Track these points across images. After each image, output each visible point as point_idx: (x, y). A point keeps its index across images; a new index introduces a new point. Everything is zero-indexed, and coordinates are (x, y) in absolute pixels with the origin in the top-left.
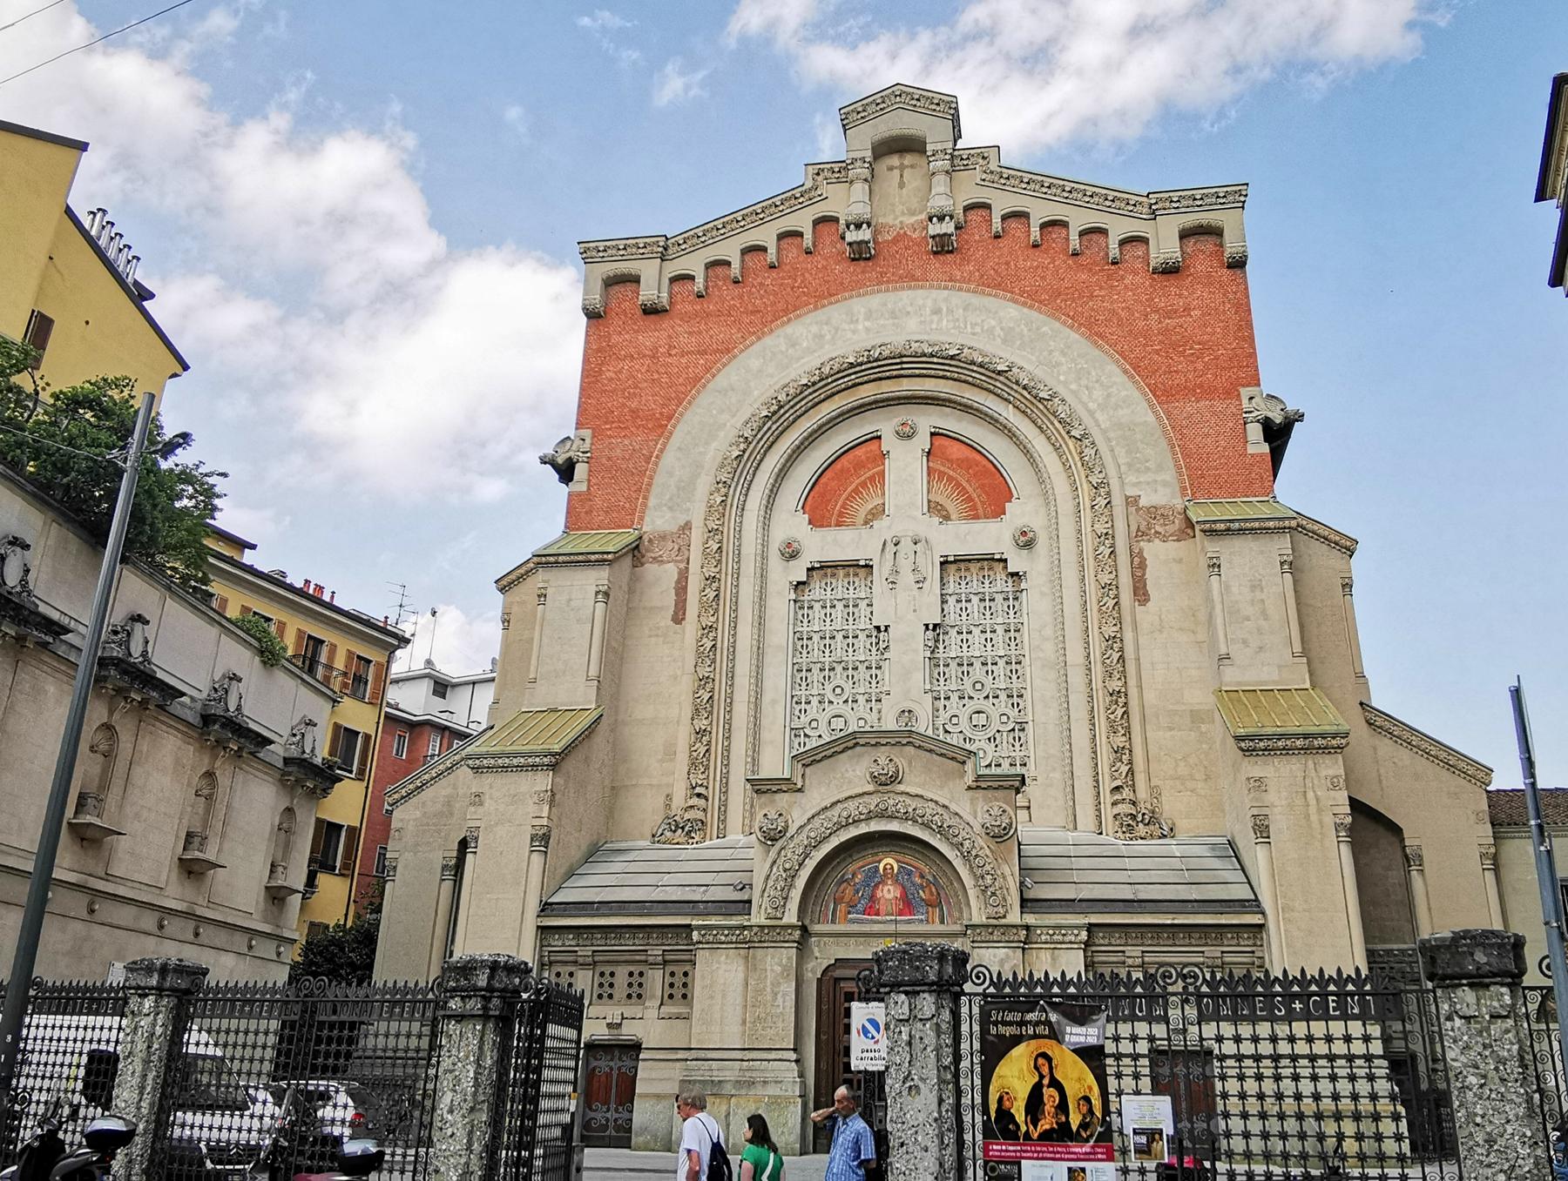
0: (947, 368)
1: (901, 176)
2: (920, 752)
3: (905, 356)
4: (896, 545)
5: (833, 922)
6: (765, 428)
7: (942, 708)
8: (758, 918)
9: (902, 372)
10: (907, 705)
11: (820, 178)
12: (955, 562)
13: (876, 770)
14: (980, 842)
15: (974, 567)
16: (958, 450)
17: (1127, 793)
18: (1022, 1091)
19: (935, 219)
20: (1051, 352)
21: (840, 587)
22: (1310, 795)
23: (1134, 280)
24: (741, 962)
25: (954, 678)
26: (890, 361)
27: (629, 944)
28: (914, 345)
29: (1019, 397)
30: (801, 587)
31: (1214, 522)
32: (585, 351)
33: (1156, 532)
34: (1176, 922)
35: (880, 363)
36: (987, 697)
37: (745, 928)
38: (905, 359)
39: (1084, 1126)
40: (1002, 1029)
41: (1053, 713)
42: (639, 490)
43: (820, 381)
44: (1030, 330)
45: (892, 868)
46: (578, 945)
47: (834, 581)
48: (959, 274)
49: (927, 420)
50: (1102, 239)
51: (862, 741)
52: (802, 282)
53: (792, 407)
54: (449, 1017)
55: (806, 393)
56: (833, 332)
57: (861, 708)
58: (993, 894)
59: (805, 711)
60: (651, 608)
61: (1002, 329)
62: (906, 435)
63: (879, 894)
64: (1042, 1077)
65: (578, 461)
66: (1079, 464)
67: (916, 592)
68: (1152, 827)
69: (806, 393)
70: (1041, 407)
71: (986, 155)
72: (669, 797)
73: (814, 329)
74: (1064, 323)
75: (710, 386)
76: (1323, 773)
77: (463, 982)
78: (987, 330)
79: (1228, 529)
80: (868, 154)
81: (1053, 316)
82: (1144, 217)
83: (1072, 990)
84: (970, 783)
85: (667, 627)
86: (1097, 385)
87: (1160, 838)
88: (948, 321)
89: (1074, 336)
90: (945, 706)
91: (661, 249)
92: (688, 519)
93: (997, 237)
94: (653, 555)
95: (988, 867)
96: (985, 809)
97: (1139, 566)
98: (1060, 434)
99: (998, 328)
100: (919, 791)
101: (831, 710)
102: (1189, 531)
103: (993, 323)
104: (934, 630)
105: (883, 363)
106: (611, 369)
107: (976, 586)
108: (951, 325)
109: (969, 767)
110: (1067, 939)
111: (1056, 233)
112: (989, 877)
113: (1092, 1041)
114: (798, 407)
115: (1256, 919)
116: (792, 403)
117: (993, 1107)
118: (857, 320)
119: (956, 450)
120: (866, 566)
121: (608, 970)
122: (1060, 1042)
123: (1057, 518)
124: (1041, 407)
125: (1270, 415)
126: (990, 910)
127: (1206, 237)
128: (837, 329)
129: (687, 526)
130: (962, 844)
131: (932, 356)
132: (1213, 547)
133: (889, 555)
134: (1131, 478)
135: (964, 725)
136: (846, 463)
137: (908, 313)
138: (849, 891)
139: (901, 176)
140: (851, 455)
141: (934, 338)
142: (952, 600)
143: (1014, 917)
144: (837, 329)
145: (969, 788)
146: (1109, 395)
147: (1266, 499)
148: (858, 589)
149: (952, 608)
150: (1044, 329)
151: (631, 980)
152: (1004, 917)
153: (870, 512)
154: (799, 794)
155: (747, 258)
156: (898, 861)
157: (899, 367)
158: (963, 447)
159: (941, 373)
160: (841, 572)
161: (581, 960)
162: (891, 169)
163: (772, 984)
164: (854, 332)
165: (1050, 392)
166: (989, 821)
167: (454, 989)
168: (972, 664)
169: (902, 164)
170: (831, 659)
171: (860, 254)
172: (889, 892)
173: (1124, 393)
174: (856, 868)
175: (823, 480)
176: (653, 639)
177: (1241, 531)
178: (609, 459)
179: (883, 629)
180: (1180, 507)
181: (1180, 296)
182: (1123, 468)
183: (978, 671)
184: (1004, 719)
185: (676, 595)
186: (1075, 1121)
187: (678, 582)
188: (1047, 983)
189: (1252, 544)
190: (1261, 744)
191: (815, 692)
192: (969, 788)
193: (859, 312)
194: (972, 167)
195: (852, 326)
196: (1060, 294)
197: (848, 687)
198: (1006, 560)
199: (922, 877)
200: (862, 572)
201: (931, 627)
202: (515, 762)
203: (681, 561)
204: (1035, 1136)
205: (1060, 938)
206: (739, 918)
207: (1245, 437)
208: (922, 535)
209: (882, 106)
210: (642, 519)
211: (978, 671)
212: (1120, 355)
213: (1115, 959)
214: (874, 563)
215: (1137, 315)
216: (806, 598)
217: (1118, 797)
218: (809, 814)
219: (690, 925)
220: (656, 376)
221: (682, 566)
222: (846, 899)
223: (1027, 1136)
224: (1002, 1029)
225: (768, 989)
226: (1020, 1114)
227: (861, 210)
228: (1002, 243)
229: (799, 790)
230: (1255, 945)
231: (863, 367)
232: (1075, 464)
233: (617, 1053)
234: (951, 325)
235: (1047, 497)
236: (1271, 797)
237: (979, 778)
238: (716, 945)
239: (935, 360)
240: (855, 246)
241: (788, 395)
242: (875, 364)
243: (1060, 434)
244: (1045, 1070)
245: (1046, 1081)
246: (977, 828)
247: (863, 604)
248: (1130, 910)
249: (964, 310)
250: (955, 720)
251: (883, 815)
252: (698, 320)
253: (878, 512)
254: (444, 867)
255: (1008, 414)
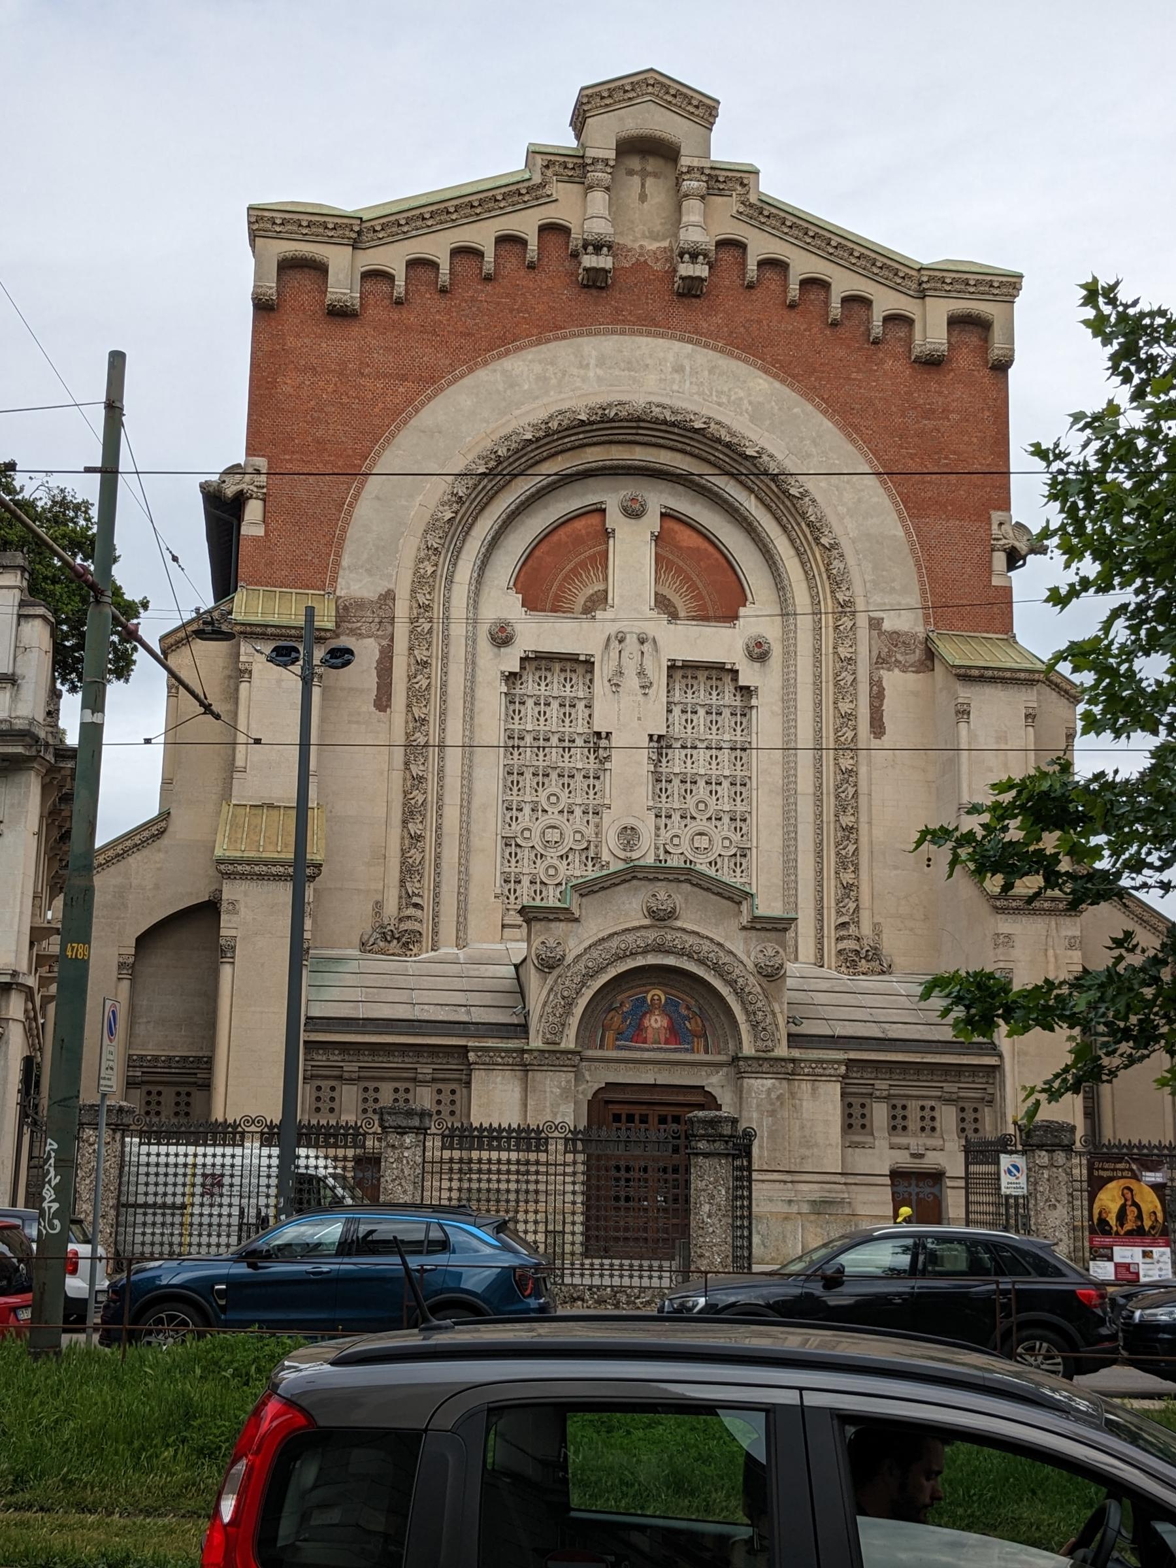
0: (687, 441)
1: (643, 185)
2: (696, 889)
3: (644, 421)
4: (620, 642)
5: (601, 1047)
6: (480, 487)
7: (663, 827)
8: (536, 1042)
9: (637, 438)
10: (630, 822)
11: (549, 173)
12: (682, 667)
13: (654, 905)
14: (752, 980)
15: (702, 675)
16: (689, 536)
17: (852, 930)
18: (1114, 1207)
19: (687, 256)
20: (802, 439)
21: (556, 686)
22: (1051, 952)
23: (892, 364)
24: (517, 1083)
25: (676, 796)
26: (626, 424)
27: (396, 1062)
28: (656, 410)
29: (764, 488)
30: (512, 679)
31: (970, 667)
32: (252, 353)
33: (896, 660)
34: (925, 1060)
35: (613, 425)
36: (710, 818)
37: (523, 1051)
38: (642, 424)
39: (1152, 1227)
40: (1102, 1173)
41: (778, 841)
42: (329, 544)
43: (545, 437)
44: (780, 409)
45: (660, 999)
46: (343, 1061)
47: (549, 675)
48: (705, 325)
49: (658, 498)
50: (863, 313)
51: (640, 875)
52: (523, 304)
53: (510, 464)
54: (697, 1154)
55: (529, 449)
56: (560, 374)
57: (578, 819)
58: (764, 1029)
59: (517, 818)
60: (351, 689)
61: (750, 403)
62: (634, 512)
63: (646, 1023)
64: (1126, 1200)
65: (251, 497)
66: (825, 576)
67: (640, 698)
68: (873, 963)
69: (529, 449)
70: (789, 504)
71: (745, 181)
72: (379, 905)
73: (538, 368)
74: (817, 407)
75: (413, 422)
76: (1064, 933)
77: (710, 1131)
78: (734, 403)
79: (982, 676)
80: (612, 155)
81: (804, 395)
82: (911, 293)
83: (1145, 1151)
84: (745, 923)
85: (370, 713)
86: (848, 486)
87: (879, 974)
88: (691, 383)
89: (828, 424)
90: (666, 825)
91: (354, 235)
92: (392, 586)
93: (751, 287)
94: (350, 626)
95: (759, 1004)
96: (759, 948)
97: (877, 696)
98: (805, 536)
99: (745, 402)
100: (696, 928)
101: (545, 820)
102: (929, 663)
103: (741, 394)
104: (658, 741)
105: (617, 424)
106: (289, 381)
107: (702, 698)
108: (695, 389)
109: (745, 907)
110: (827, 1072)
111: (814, 295)
112: (760, 1013)
113: (1160, 1180)
114: (517, 464)
115: (993, 1061)
116: (511, 460)
117: (1096, 1217)
118: (588, 365)
119: (688, 538)
120: (586, 662)
121: (371, 1085)
122: (1139, 1180)
123: (795, 632)
124: (789, 504)
125: (1017, 544)
126: (759, 1043)
127: (971, 327)
128: (564, 373)
129: (389, 597)
130: (736, 982)
131: (673, 424)
132: (965, 693)
133: (614, 654)
134: (877, 598)
135: (685, 847)
136: (563, 536)
137: (647, 366)
138: (617, 1020)
139: (643, 185)
140: (568, 528)
141: (678, 404)
142: (677, 710)
143: (782, 1051)
144: (564, 373)
145: (744, 928)
146: (859, 500)
147: (1005, 637)
148: (575, 688)
149: (677, 718)
150: (795, 410)
151: (375, 1095)
152: (773, 1050)
153: (590, 599)
154: (575, 925)
155: (457, 260)
156: (665, 993)
157: (634, 431)
158: (694, 535)
159: (680, 446)
160: (557, 667)
161: (346, 1075)
162: (631, 173)
163: (552, 1105)
164: (584, 379)
165: (801, 490)
166: (762, 961)
167: (703, 1136)
168: (695, 783)
169: (644, 169)
170: (545, 764)
171: (596, 281)
172: (656, 1022)
173: (875, 499)
174: (625, 999)
175: (537, 553)
176: (354, 726)
177: (993, 680)
178: (291, 499)
179: (604, 735)
180: (922, 636)
181: (940, 393)
182: (868, 585)
183: (701, 789)
184: (727, 843)
185: (379, 677)
186: (1147, 1224)
187: (379, 662)
188: (1130, 1146)
189: (1002, 694)
190: (1014, 904)
191: (528, 798)
192: (744, 928)
193: (590, 355)
194: (728, 193)
195: (582, 372)
196: (815, 370)
197: (564, 795)
198: (737, 671)
199: (688, 1008)
200: (581, 670)
201: (655, 738)
202: (274, 870)
203: (382, 637)
204: (1122, 1233)
205: (821, 1071)
206: (516, 1041)
207: (990, 567)
208: (651, 634)
209: (631, 95)
210: (334, 580)
211: (701, 789)
212: (874, 454)
213: (864, 1091)
214: (597, 660)
215: (893, 409)
216: (517, 691)
217: (843, 933)
218: (586, 944)
219: (466, 1046)
220: (345, 400)
221: (385, 643)
222: (615, 1026)
223: (1117, 1233)
224: (1102, 1173)
225: (548, 1110)
226: (1112, 1220)
227: (600, 228)
228: (758, 293)
229: (577, 920)
230: (987, 1083)
231: (595, 427)
232: (820, 575)
233: (914, 1182)
234: (695, 389)
235: (786, 613)
236: (1017, 953)
237: (755, 919)
238: (490, 1066)
239: (676, 430)
240: (592, 274)
241: (509, 450)
242: (608, 425)
243: (805, 536)
244: (1129, 1196)
245: (1130, 1201)
246: (750, 966)
247: (581, 705)
248: (893, 1048)
249: (710, 372)
250: (676, 841)
251: (659, 949)
252: (395, 333)
253: (600, 600)
254: (121, 966)
255: (750, 505)
